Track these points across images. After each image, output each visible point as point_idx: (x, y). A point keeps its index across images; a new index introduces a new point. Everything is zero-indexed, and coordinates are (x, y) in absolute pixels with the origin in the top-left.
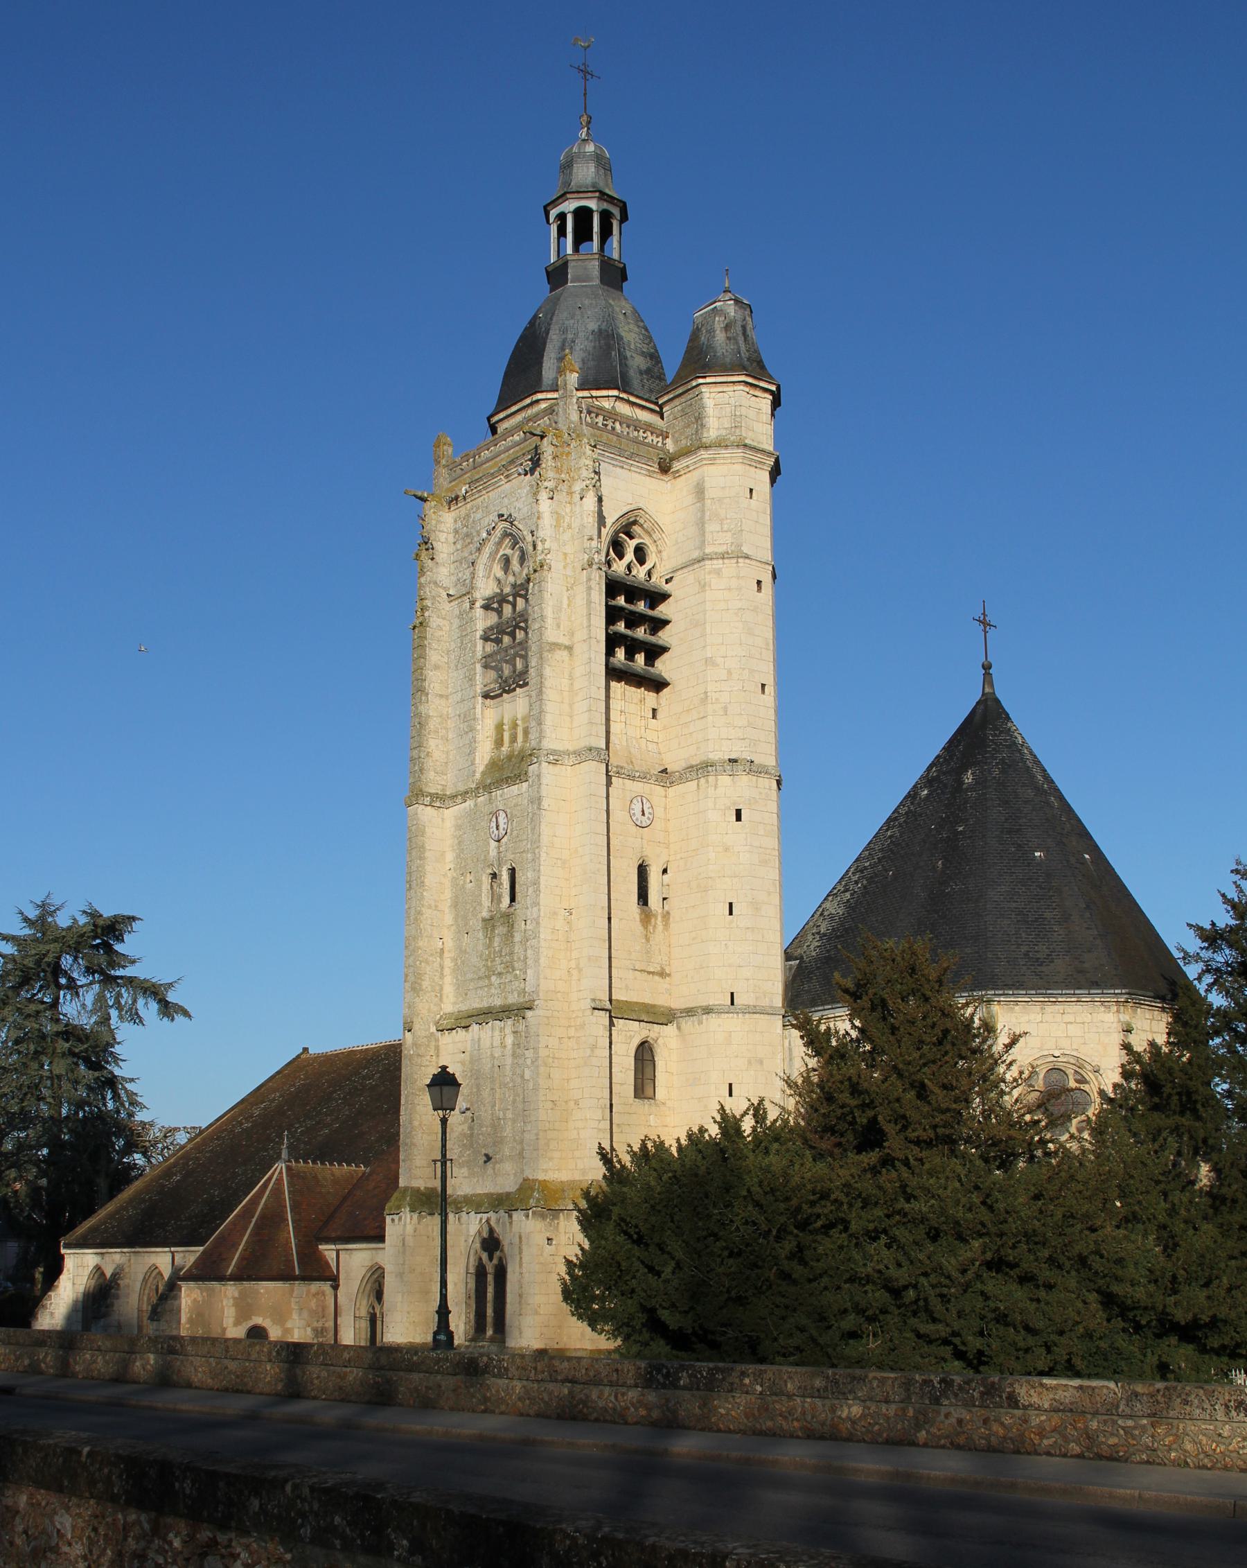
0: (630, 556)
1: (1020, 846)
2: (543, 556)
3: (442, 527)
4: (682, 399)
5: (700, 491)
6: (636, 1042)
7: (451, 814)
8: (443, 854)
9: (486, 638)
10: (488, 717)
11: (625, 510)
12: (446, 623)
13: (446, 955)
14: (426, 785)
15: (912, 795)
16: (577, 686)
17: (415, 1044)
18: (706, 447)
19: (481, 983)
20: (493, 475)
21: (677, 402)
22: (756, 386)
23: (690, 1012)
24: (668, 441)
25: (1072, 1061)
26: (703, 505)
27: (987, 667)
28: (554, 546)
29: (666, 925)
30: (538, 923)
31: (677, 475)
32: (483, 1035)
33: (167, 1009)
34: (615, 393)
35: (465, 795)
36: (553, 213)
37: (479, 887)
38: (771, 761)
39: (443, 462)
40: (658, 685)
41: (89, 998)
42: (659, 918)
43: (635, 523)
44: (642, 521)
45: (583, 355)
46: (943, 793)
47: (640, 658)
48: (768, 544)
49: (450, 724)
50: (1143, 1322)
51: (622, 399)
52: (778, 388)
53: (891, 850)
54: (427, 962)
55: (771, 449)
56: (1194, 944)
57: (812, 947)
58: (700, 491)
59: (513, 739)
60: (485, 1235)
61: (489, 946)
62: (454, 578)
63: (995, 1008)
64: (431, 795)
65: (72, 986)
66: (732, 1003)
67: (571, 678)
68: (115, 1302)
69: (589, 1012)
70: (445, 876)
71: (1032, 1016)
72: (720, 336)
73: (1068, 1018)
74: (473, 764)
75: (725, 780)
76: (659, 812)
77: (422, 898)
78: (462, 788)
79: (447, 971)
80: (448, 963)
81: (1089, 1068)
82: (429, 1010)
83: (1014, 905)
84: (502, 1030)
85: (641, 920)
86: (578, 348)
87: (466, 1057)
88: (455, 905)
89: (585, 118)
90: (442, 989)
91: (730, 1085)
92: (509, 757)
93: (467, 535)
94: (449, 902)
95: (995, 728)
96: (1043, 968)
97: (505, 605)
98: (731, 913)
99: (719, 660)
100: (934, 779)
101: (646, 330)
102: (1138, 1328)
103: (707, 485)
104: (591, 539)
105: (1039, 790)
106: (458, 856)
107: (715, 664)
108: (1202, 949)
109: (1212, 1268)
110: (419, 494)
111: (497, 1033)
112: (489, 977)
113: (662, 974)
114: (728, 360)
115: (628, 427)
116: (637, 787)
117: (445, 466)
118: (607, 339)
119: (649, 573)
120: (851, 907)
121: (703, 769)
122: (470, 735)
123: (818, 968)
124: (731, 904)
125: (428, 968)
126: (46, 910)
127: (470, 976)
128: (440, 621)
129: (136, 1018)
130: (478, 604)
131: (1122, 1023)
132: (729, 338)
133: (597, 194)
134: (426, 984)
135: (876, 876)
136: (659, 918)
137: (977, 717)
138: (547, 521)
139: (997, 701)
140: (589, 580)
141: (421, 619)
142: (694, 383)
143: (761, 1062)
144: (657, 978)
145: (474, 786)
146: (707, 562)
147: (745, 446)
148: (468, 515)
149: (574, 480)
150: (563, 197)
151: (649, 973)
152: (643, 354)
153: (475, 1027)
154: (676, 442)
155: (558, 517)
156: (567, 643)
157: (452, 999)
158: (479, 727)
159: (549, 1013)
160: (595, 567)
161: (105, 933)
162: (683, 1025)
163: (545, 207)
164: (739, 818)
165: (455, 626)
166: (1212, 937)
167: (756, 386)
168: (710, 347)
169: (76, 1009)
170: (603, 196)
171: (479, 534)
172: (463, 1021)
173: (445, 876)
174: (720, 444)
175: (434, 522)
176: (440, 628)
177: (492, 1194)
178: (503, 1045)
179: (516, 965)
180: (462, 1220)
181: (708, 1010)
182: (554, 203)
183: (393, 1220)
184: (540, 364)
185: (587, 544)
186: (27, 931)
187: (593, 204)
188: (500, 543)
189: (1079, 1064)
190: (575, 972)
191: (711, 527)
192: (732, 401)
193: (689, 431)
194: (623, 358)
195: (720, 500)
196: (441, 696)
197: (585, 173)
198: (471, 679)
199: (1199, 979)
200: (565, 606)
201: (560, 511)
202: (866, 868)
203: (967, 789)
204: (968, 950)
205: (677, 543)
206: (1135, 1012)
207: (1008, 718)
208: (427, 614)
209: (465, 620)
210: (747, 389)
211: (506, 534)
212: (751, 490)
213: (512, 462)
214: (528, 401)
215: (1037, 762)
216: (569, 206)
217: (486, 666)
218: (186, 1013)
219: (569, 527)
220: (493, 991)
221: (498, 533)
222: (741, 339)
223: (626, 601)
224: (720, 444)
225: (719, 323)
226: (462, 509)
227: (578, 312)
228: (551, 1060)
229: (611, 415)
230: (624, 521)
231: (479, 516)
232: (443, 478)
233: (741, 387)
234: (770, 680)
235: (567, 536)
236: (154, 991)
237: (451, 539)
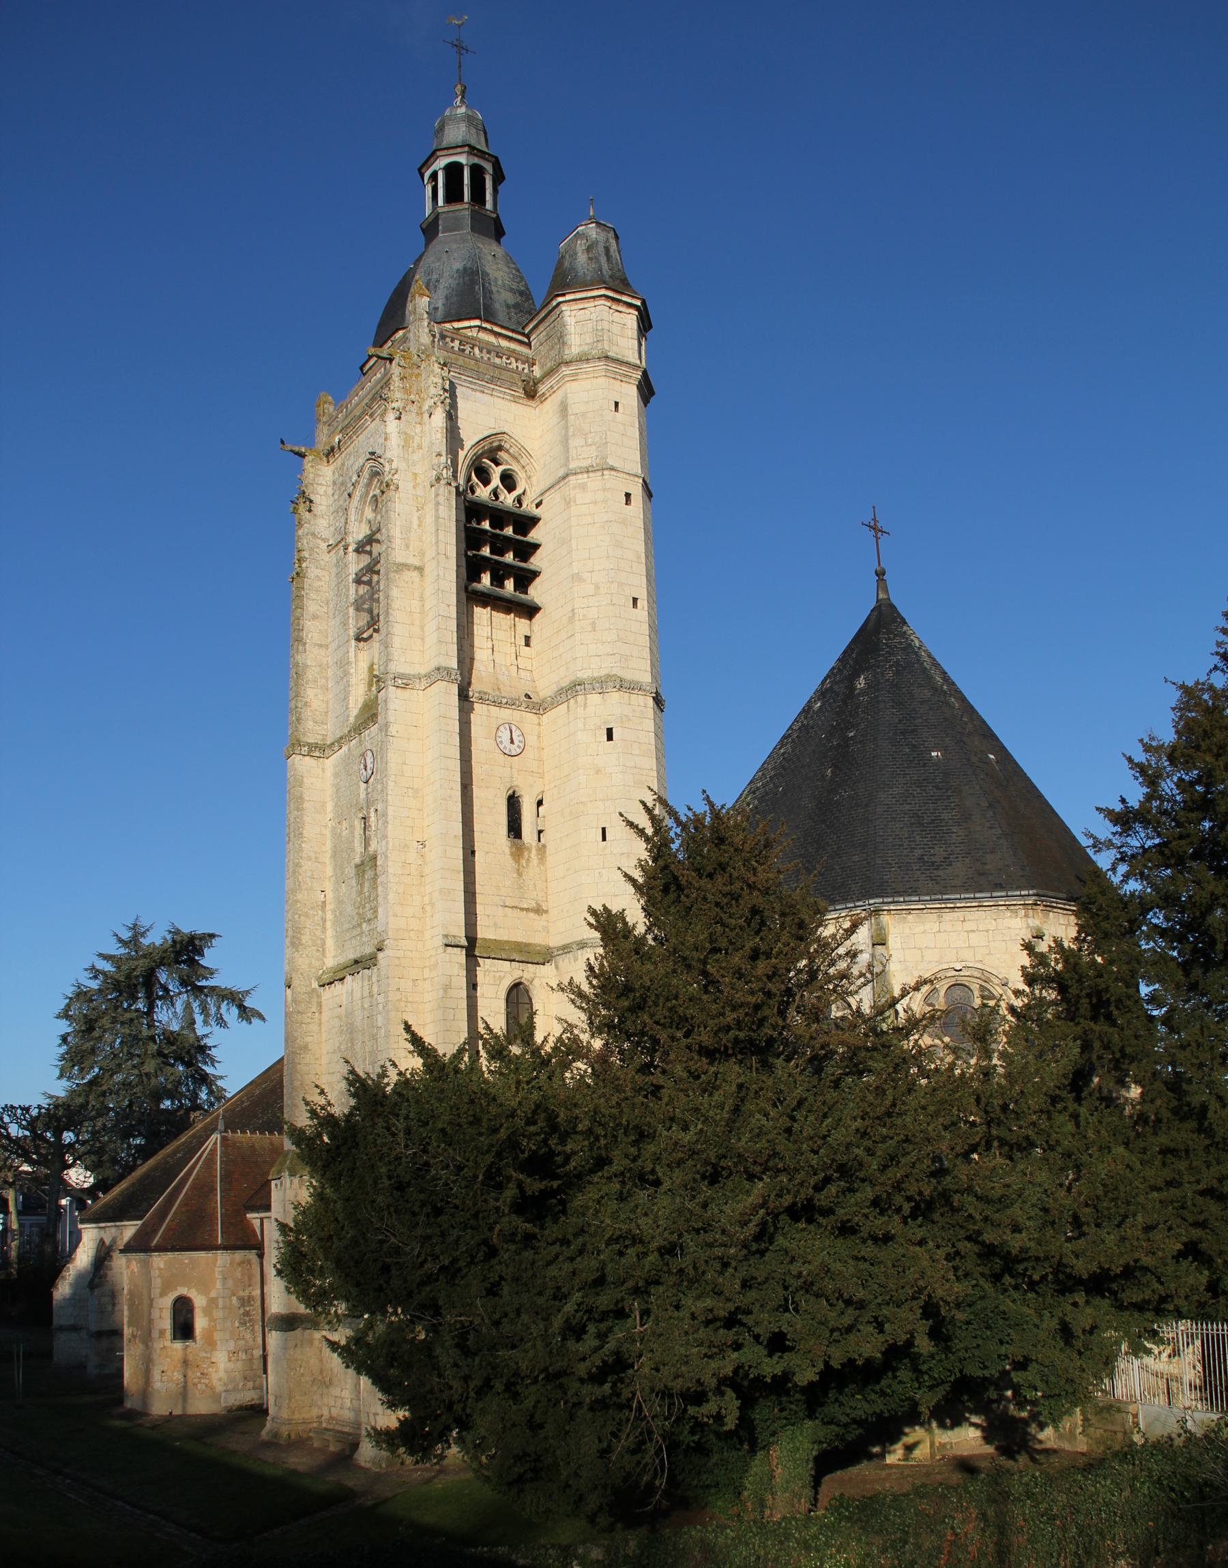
0: (496, 481)
1: (914, 746)
3: (321, 480)
4: (546, 324)
5: (564, 409)
6: (507, 983)
7: (331, 763)
8: (324, 804)
11: (486, 434)
12: (325, 573)
13: (329, 907)
14: (304, 734)
15: (806, 711)
16: (427, 606)
18: (567, 363)
20: (360, 418)
21: (541, 328)
22: (619, 301)
24: (536, 368)
25: (976, 974)
27: (880, 574)
28: (402, 466)
30: (386, 857)
33: (246, 1014)
34: (477, 322)
36: (427, 175)
37: (352, 833)
38: (646, 678)
40: (530, 611)
41: (179, 1005)
42: (534, 852)
43: (500, 448)
44: (507, 446)
45: (446, 292)
46: (835, 702)
47: (509, 584)
48: (637, 456)
49: (330, 673)
50: (1036, 1277)
51: (485, 329)
52: (644, 302)
53: (783, 767)
54: (307, 915)
55: (633, 358)
56: (1105, 830)
61: (361, 893)
62: (332, 529)
63: (885, 919)
64: (309, 744)
65: (167, 997)
67: (422, 599)
68: (109, 1273)
69: (441, 950)
71: (928, 926)
72: (582, 258)
73: (969, 926)
75: (594, 698)
76: (531, 740)
77: (301, 849)
79: (328, 924)
80: (329, 916)
81: (996, 981)
83: (908, 807)
84: (370, 977)
85: (512, 854)
86: (441, 287)
87: (342, 1011)
88: (334, 855)
89: (459, 87)
93: (342, 484)
95: (889, 632)
96: (940, 873)
98: (604, 839)
99: (586, 576)
100: (827, 690)
101: (518, 270)
102: (1032, 1285)
103: (570, 401)
104: (439, 455)
105: (936, 690)
106: (336, 805)
108: (1114, 834)
109: (1128, 1203)
110: (296, 449)
111: (366, 983)
112: (360, 925)
113: (538, 910)
114: (589, 278)
115: (489, 352)
116: (506, 714)
117: (325, 423)
118: (472, 278)
119: (519, 500)
121: (573, 689)
124: (604, 830)
126: (138, 931)
127: (346, 926)
128: (319, 572)
129: (221, 1022)
130: (351, 549)
131: (1031, 928)
132: (590, 259)
133: (466, 149)
134: (305, 938)
135: (767, 794)
136: (534, 852)
137: (871, 624)
138: (395, 441)
139: (892, 607)
140: (437, 495)
142: (554, 303)
144: (531, 914)
146: (571, 478)
147: (607, 357)
148: (343, 464)
150: (433, 156)
151: (522, 909)
152: (511, 290)
153: (349, 978)
154: (542, 367)
155: (407, 439)
156: (417, 564)
158: (352, 671)
159: (400, 954)
160: (443, 482)
161: (187, 951)
162: (561, 964)
163: (420, 170)
164: (610, 736)
165: (333, 575)
166: (1124, 819)
167: (619, 301)
168: (572, 268)
169: (168, 1017)
170: (473, 150)
171: (351, 478)
174: (584, 359)
175: (311, 476)
176: (318, 578)
182: (427, 163)
185: (435, 461)
186: (123, 951)
187: (462, 159)
188: (369, 485)
189: (985, 976)
191: (575, 442)
192: (594, 317)
193: (553, 353)
194: (488, 293)
195: (584, 415)
196: (321, 646)
198: (345, 624)
199: (1114, 869)
201: (409, 431)
202: (758, 788)
204: (856, 858)
206: (1047, 917)
207: (904, 622)
208: (304, 565)
209: (341, 565)
210: (609, 304)
212: (617, 404)
215: (936, 665)
216: (441, 163)
217: (358, 609)
218: (262, 1018)
219: (420, 447)
220: (364, 939)
221: (366, 474)
222: (603, 259)
223: (491, 526)
224: (584, 359)
225: (581, 246)
226: (339, 459)
227: (445, 255)
228: (403, 1004)
229: (473, 342)
230: (486, 445)
231: (351, 462)
233: (602, 302)
235: (416, 457)
236: (235, 998)
237: (330, 491)
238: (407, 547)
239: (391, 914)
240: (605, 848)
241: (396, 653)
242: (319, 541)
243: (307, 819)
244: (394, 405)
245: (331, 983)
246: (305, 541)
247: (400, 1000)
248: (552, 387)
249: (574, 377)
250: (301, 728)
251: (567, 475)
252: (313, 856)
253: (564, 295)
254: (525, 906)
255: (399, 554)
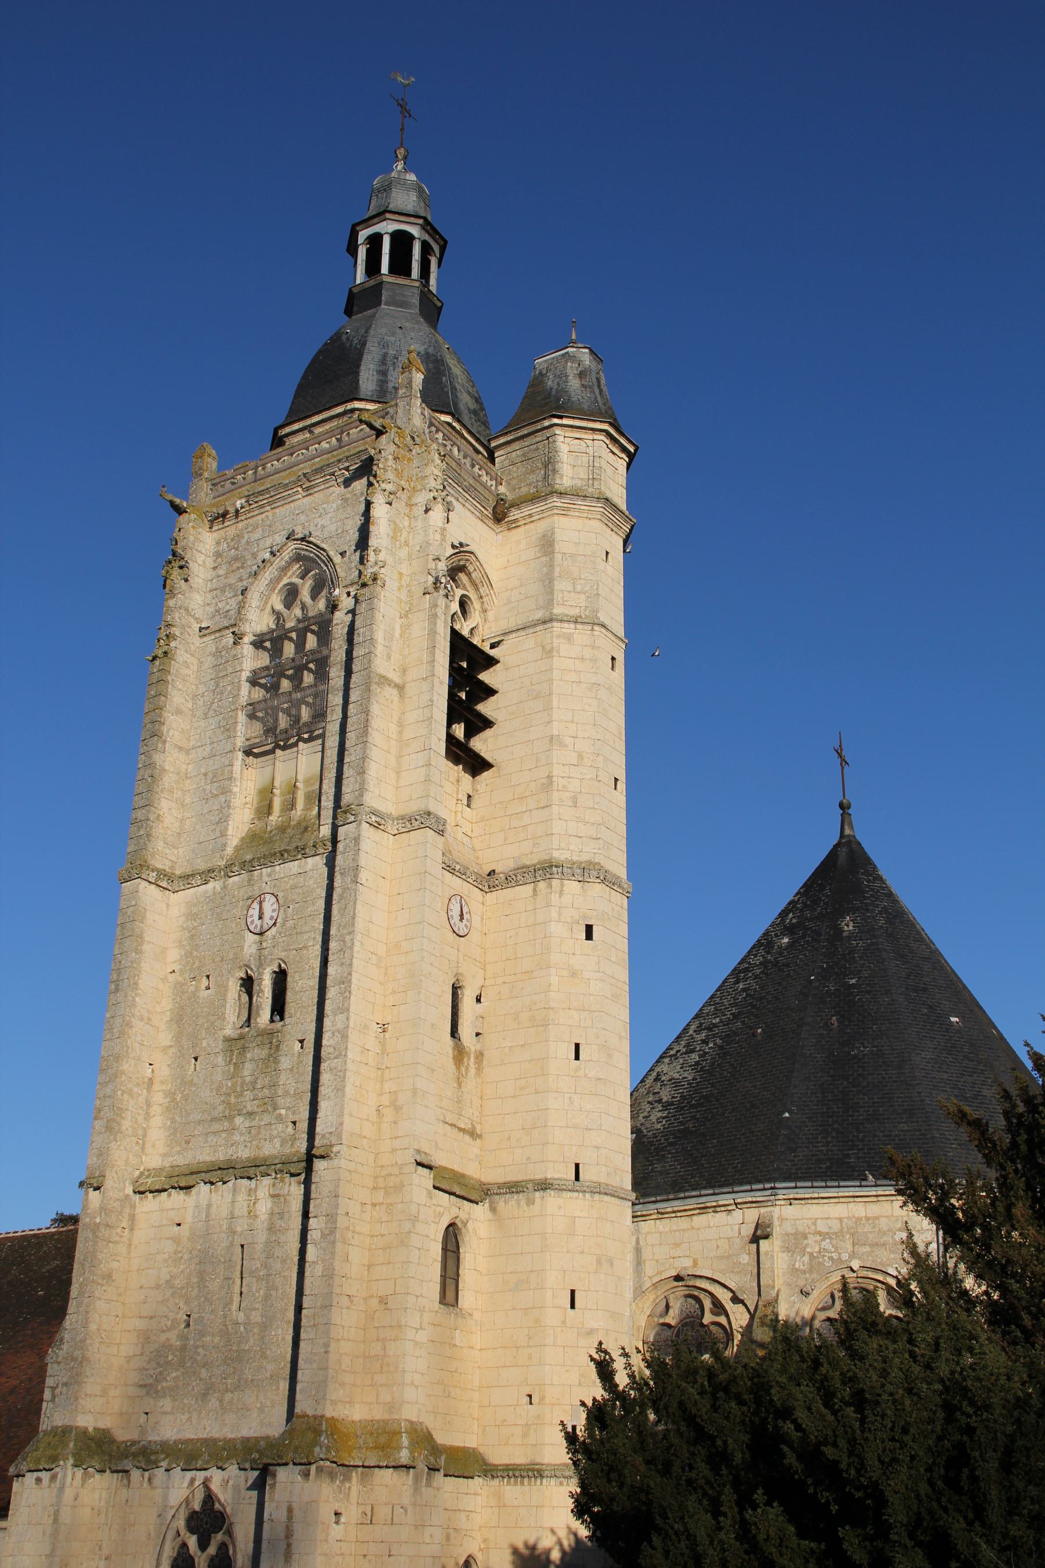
2: (376, 569)
4: (527, 442)
7: (179, 901)
8: (164, 950)
9: (253, 682)
10: (247, 781)
13: (156, 1087)
15: (765, 943)
16: (408, 734)
17: (103, 1209)
19: (216, 1126)
20: (286, 487)
21: (516, 446)
23: (514, 1188)
26: (552, 560)
28: (390, 561)
29: (479, 1069)
31: (513, 525)
32: (215, 1198)
35: (208, 875)
36: (363, 235)
39: (206, 475)
40: (477, 765)
42: (472, 1059)
44: (471, 568)
57: (653, 1118)
58: (547, 545)
59: (290, 805)
60: (197, 1506)
62: (210, 609)
66: (577, 1178)
70: (164, 980)
74: (223, 834)
76: (476, 920)
77: (134, 1005)
78: (202, 865)
79: (156, 1110)
80: (159, 1098)
82: (127, 1161)
85: (454, 1058)
88: (179, 1018)
90: (145, 1135)
91: (573, 1292)
92: (282, 829)
94: (168, 1016)
97: (286, 642)
98: (577, 1058)
99: (568, 741)
106: (188, 954)
107: (562, 745)
110: (178, 501)
111: (242, 1198)
112: (230, 1118)
113: (473, 1134)
117: (207, 480)
120: (705, 1071)
121: (546, 870)
122: (222, 798)
123: (671, 1144)
124: (577, 1046)
125: (132, 1103)
127: (196, 1116)
130: (248, 639)
133: (421, 221)
134: (126, 1124)
135: (735, 1034)
136: (472, 1059)
141: (166, 648)
142: (546, 423)
143: (611, 1263)
144: (467, 1138)
145: (223, 863)
146: (555, 624)
148: (239, 536)
149: (415, 490)
150: (381, 215)
153: (204, 1189)
155: (396, 529)
156: (397, 680)
157: (162, 1149)
158: (235, 789)
164: (589, 936)
170: (428, 226)
171: (254, 556)
172: (182, 1181)
173: (164, 980)
174: (577, 494)
175: (191, 538)
177: (215, 1441)
178: (252, 1214)
179: (281, 1101)
180: (156, 1481)
181: (544, 1186)
182: (367, 222)
183: (39, 1480)
184: (356, 374)
185: (432, 565)
187: (415, 231)
188: (284, 570)
190: (389, 1113)
191: (559, 585)
192: (590, 451)
195: (573, 556)
196: (181, 749)
197: (405, 199)
198: (229, 730)
200: (397, 634)
202: (715, 1025)
203: (849, 938)
205: (509, 602)
208: (173, 644)
209: (223, 662)
210: (608, 442)
211: (298, 558)
212: (607, 553)
213: (320, 470)
214: (340, 409)
216: (387, 227)
217: (252, 716)
219: (407, 544)
220: (237, 1137)
221: (287, 554)
225: (571, 369)
226: (232, 529)
227: (399, 331)
231: (258, 534)
232: (203, 494)
234: (622, 776)
238: (389, 658)
239: (346, 1112)
240: (577, 1069)
241: (371, 784)
242: (192, 620)
243: (145, 966)
244: (383, 486)
245: (159, 1191)
246: (177, 615)
247: (347, 1228)
248: (530, 516)
249: (565, 512)
250: (150, 845)
251: (551, 620)
252: (146, 1015)
253: (561, 417)
254: (462, 1126)
255: (382, 665)
